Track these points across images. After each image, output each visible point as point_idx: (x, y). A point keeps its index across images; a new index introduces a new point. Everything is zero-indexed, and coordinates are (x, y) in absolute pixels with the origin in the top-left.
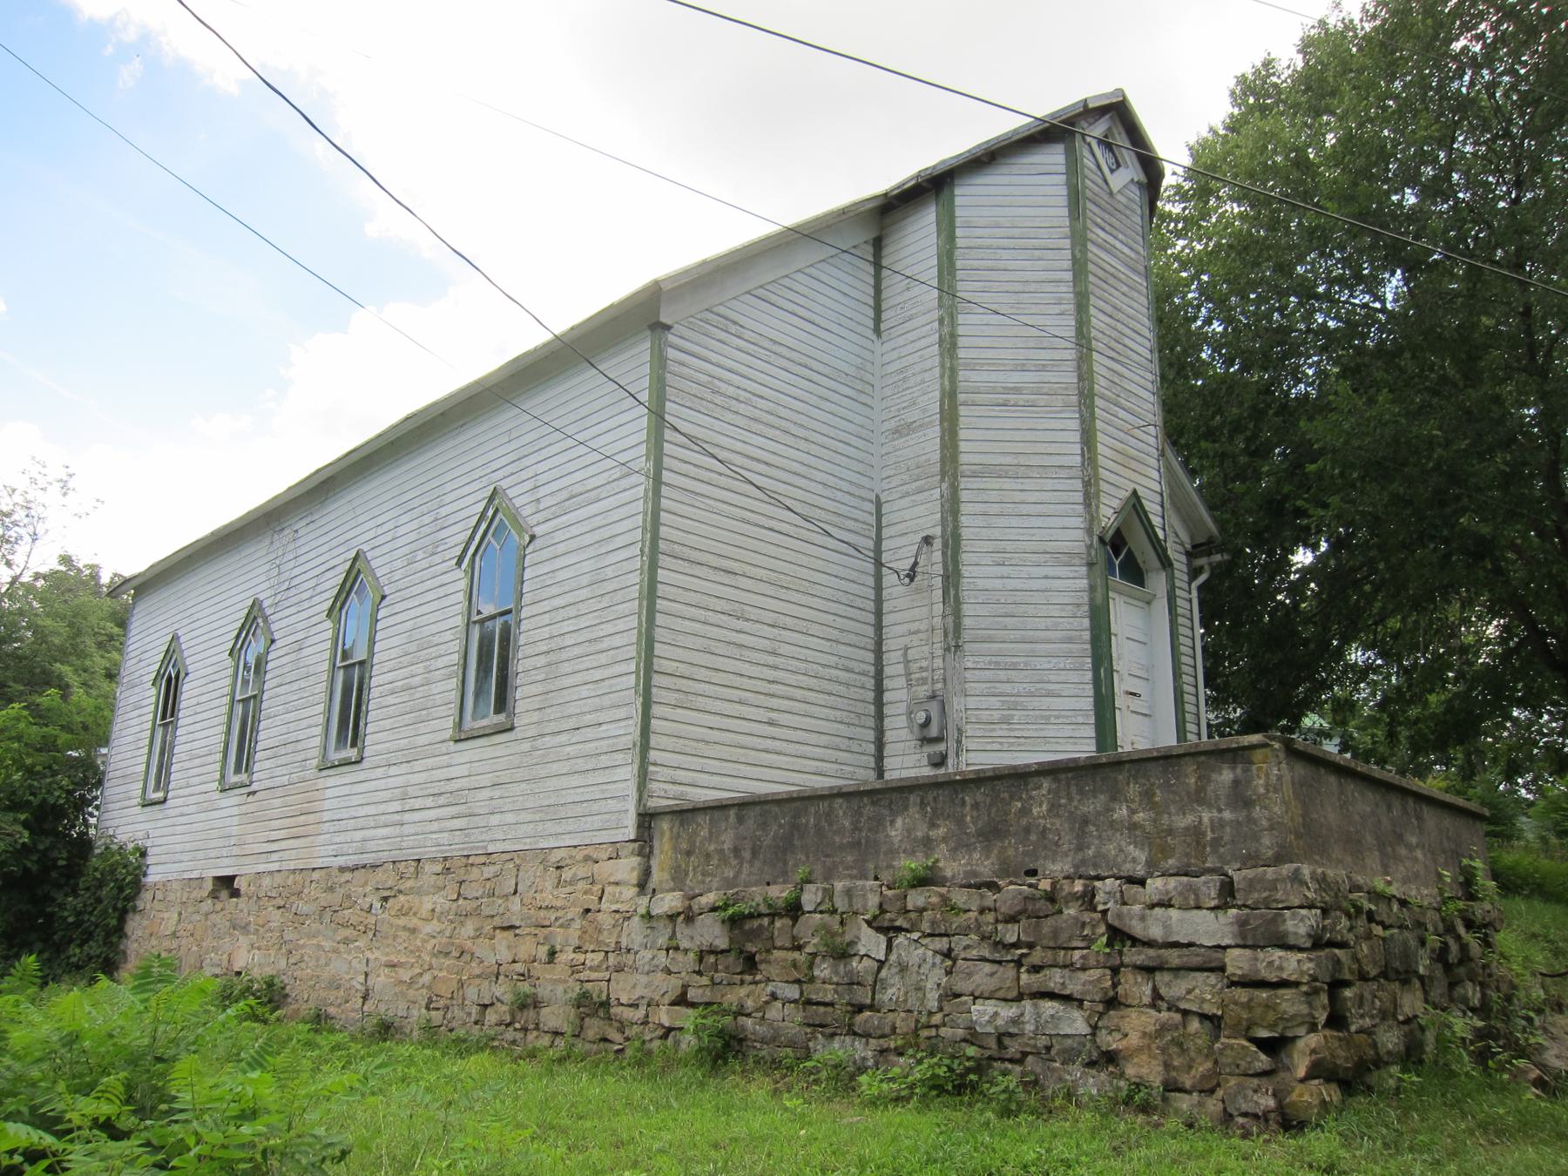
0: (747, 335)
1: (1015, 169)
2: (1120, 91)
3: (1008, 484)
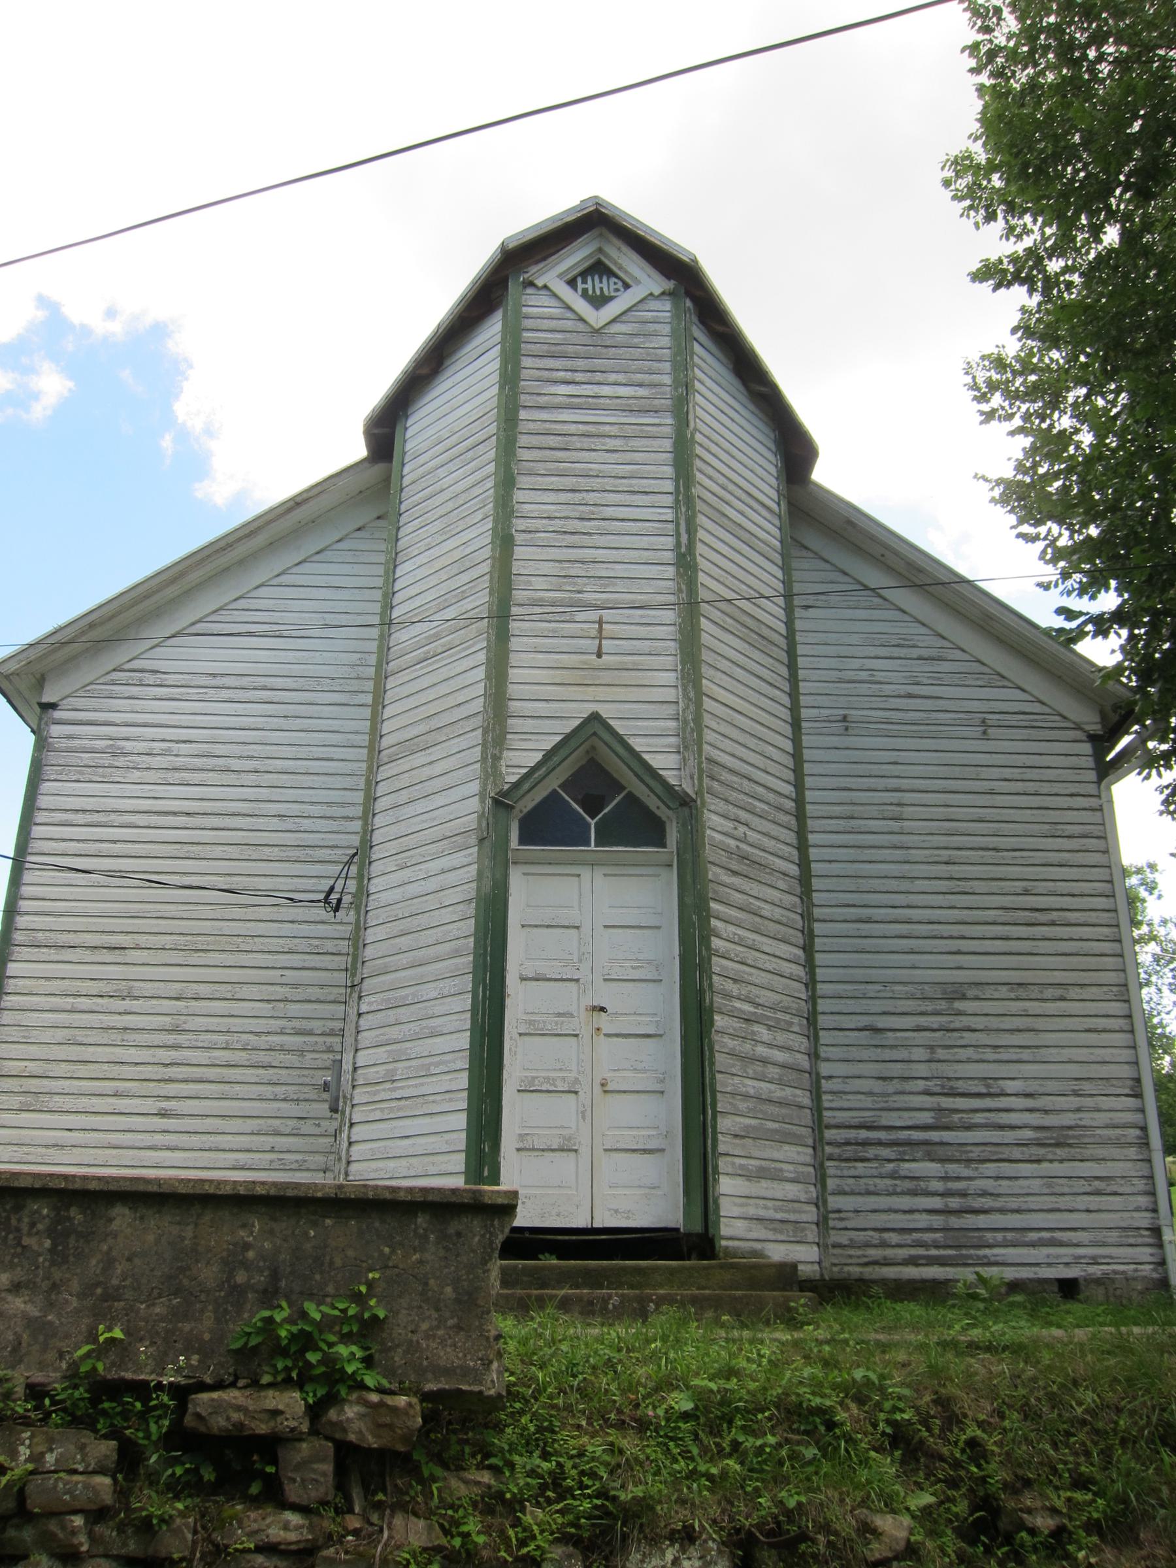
0: (171, 679)
1: (459, 365)
2: (597, 202)
3: (420, 759)
